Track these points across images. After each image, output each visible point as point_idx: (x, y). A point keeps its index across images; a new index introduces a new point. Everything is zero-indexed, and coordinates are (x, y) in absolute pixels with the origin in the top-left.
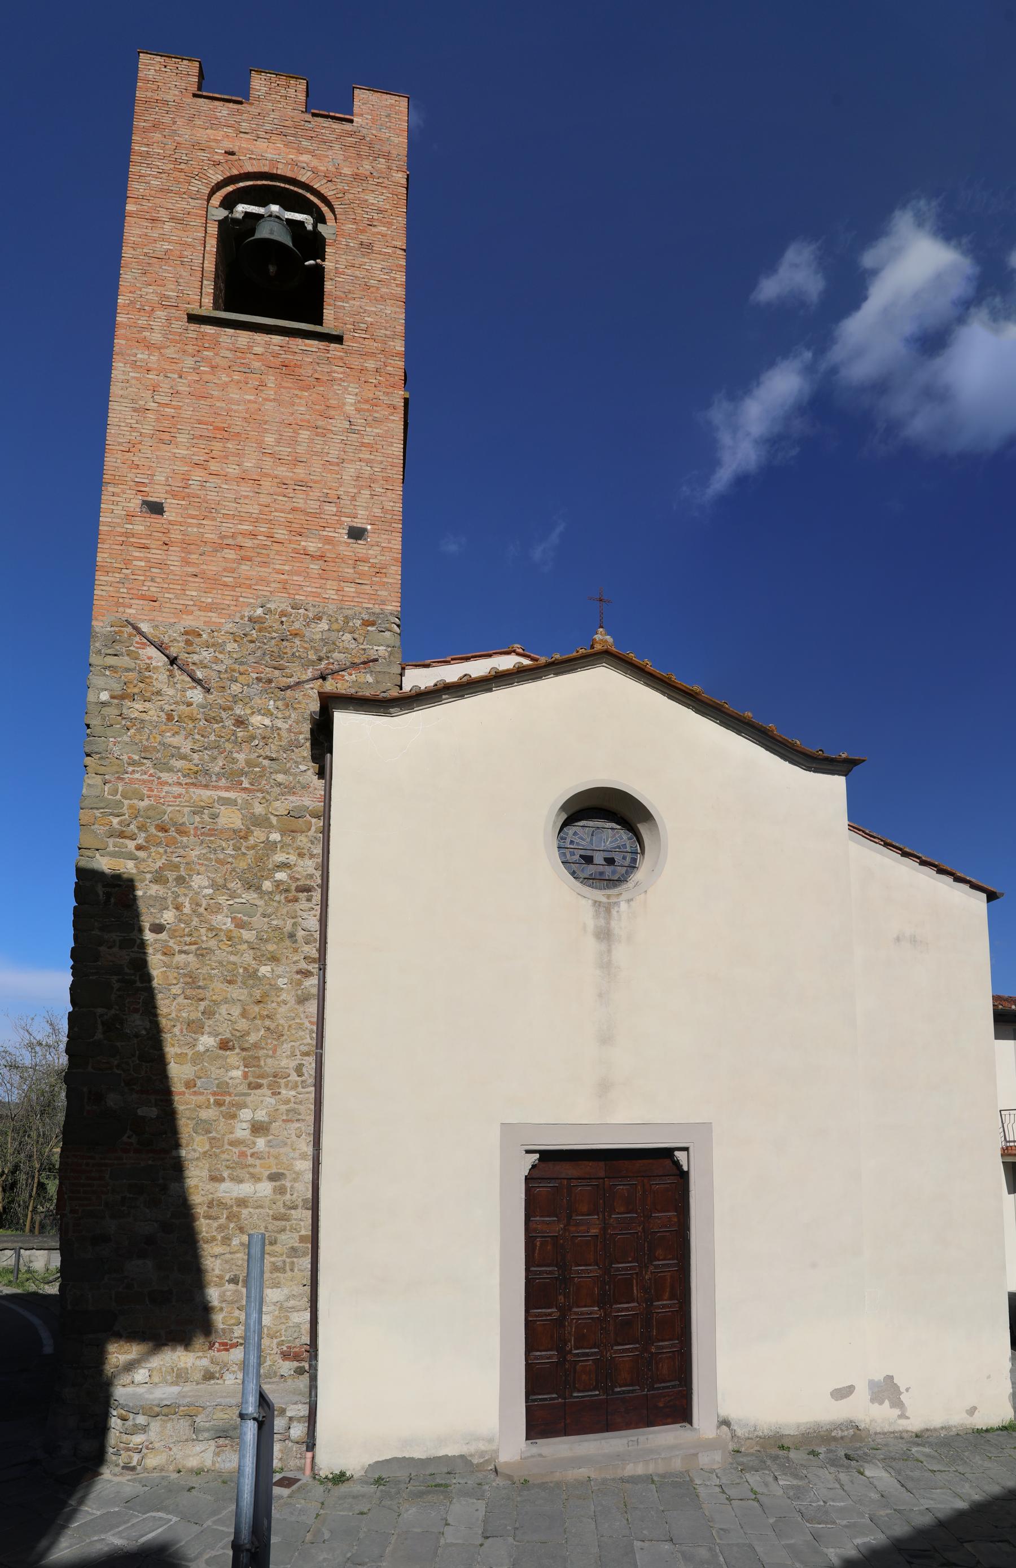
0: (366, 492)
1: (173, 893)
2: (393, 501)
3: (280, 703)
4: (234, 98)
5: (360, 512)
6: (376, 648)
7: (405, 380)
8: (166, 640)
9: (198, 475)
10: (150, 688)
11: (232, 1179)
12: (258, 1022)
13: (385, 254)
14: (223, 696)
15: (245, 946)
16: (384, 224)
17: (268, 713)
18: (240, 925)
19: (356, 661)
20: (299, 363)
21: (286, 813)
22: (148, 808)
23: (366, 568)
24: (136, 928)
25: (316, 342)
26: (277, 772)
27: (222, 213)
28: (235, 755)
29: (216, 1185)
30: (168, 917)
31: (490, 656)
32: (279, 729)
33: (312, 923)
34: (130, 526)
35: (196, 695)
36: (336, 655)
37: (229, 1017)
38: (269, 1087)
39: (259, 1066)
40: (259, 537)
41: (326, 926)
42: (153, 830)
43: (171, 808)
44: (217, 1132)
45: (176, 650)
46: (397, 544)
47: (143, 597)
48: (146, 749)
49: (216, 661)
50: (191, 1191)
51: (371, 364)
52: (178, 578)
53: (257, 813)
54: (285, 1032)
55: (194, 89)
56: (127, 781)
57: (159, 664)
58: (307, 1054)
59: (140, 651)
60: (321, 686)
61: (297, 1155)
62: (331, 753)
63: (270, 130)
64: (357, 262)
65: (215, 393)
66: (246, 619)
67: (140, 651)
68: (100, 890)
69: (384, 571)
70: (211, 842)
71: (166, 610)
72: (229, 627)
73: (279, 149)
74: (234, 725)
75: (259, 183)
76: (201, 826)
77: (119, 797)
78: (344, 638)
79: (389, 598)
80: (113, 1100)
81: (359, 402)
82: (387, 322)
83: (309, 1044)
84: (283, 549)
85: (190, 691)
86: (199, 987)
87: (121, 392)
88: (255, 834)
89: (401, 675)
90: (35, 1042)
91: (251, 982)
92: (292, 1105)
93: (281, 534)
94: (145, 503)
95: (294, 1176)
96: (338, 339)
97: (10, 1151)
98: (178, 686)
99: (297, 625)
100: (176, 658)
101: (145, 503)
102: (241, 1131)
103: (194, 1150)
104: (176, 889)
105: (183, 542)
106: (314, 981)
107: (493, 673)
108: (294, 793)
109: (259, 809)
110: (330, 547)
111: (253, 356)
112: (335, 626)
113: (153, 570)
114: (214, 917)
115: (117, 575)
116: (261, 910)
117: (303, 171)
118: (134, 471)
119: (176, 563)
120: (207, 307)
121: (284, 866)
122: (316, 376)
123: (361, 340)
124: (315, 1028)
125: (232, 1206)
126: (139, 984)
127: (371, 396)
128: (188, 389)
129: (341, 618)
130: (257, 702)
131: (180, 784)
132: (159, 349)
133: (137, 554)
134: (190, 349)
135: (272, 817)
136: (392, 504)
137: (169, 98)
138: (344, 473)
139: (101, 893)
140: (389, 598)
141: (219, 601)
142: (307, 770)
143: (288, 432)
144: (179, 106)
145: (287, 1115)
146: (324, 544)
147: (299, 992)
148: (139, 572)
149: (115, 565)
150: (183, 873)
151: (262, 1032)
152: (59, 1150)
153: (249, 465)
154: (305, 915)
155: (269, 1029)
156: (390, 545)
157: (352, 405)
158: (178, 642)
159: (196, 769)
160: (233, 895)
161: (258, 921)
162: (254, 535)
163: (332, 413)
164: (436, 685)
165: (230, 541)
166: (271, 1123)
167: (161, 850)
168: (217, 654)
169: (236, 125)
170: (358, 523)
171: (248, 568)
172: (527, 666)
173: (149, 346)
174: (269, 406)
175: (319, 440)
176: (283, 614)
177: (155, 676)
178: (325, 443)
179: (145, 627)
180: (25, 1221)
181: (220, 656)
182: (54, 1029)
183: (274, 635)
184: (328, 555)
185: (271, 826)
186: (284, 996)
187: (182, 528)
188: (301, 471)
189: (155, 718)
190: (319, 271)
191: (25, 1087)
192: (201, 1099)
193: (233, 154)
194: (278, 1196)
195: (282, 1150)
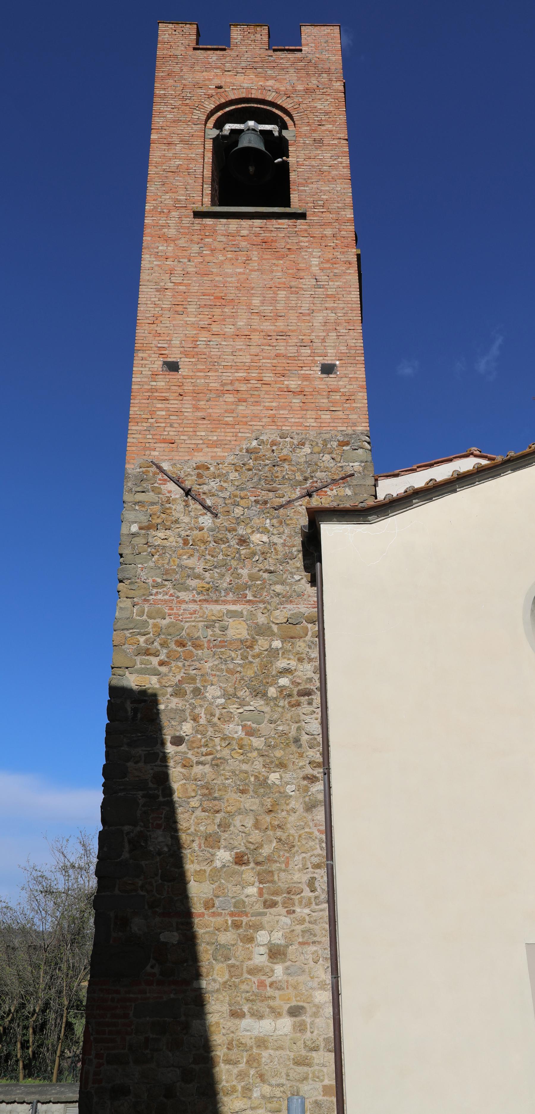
0: (333, 334)
1: (190, 704)
2: (355, 339)
3: (275, 521)
4: (220, 47)
5: (329, 351)
6: (351, 464)
7: (356, 240)
8: (182, 475)
9: (204, 336)
10: (170, 518)
11: (252, 1015)
12: (270, 833)
13: (333, 145)
14: (228, 520)
15: (255, 754)
16: (330, 123)
17: (265, 531)
18: (250, 733)
19: (336, 477)
20: (274, 239)
21: (285, 620)
22: (169, 626)
23: (338, 397)
24: (159, 742)
25: (286, 221)
26: (276, 583)
27: (215, 133)
28: (240, 571)
29: (237, 1021)
30: (187, 728)
31: (450, 460)
32: (275, 544)
33: (315, 727)
34: (154, 383)
35: (206, 520)
36: (318, 474)
37: (243, 831)
38: (284, 904)
39: (273, 882)
40: (251, 382)
41: (327, 729)
42: (173, 646)
43: (187, 624)
44: (236, 958)
45: (190, 483)
46: (361, 373)
47: (164, 441)
48: (167, 572)
49: (222, 489)
50: (213, 1029)
51: (328, 232)
52: (190, 422)
53: (261, 623)
54: (296, 843)
55: (193, 44)
56: (152, 602)
57: (177, 496)
58: (317, 866)
59: (162, 487)
60: (308, 503)
61: (315, 985)
62: (321, 562)
63: (246, 66)
64: (312, 155)
65: (214, 270)
66: (244, 451)
67: (162, 487)
68: (129, 706)
69: (353, 397)
70: (222, 653)
71: (182, 450)
72: (231, 459)
73: (251, 79)
74: (238, 544)
75: (239, 106)
76: (213, 639)
77: (145, 617)
78: (324, 459)
79: (359, 420)
80: (138, 925)
81: (322, 262)
82: (338, 197)
83: (319, 855)
84: (271, 389)
85: (202, 517)
86: (215, 799)
87: (148, 278)
88: (260, 642)
89: (375, 486)
90: (68, 864)
91: (262, 790)
92: (307, 925)
93: (269, 376)
94: (165, 363)
95: (314, 1009)
96: (302, 216)
97: (42, 986)
98: (192, 514)
99: (285, 452)
100: (190, 490)
101: (165, 363)
102: (260, 957)
103: (214, 980)
104: (193, 701)
105: (194, 392)
106: (319, 786)
107: (455, 476)
108: (291, 602)
109: (262, 619)
110: (307, 383)
111: (240, 238)
112: (316, 449)
113: (172, 417)
114: (226, 726)
115: (144, 424)
116: (267, 716)
117: (269, 93)
118: (157, 338)
119: (189, 410)
120: (207, 204)
121: (286, 671)
122: (288, 246)
123: (320, 214)
124: (324, 837)
125: (251, 1047)
126: (161, 799)
127: (331, 256)
128: (194, 269)
129: (320, 442)
130: (256, 522)
131: (195, 601)
132: (174, 241)
133: (159, 406)
134: (196, 238)
135: (273, 626)
136: (354, 341)
137: (178, 53)
138: (314, 321)
139: (129, 709)
140: (359, 420)
141: (222, 438)
142: (301, 578)
143: (270, 294)
144: (185, 58)
145: (303, 937)
146: (303, 381)
147: (307, 799)
148: (161, 420)
149: (144, 416)
150: (199, 685)
151: (274, 844)
152: (85, 984)
153: (242, 324)
154: (307, 718)
155: (280, 840)
156: (356, 375)
157: (316, 266)
158: (192, 476)
159: (207, 586)
160: (242, 704)
161: (265, 728)
162: (247, 380)
163: (302, 274)
164: (406, 491)
165: (229, 387)
166: (287, 946)
167: (180, 664)
168: (222, 483)
169: (222, 67)
170: (328, 361)
171: (244, 408)
172: (486, 465)
173: (167, 239)
174: (254, 275)
175: (293, 297)
176: (273, 443)
177: (174, 507)
178: (298, 299)
179: (165, 466)
180: (52, 1069)
181: (225, 485)
182: (86, 850)
183: (267, 462)
184: (307, 390)
185: (273, 634)
186: (293, 804)
187: (193, 381)
188: (281, 324)
189: (174, 544)
190: (285, 165)
191: (58, 914)
192: (220, 920)
193: (220, 87)
194: (299, 1035)
195: (301, 979)
